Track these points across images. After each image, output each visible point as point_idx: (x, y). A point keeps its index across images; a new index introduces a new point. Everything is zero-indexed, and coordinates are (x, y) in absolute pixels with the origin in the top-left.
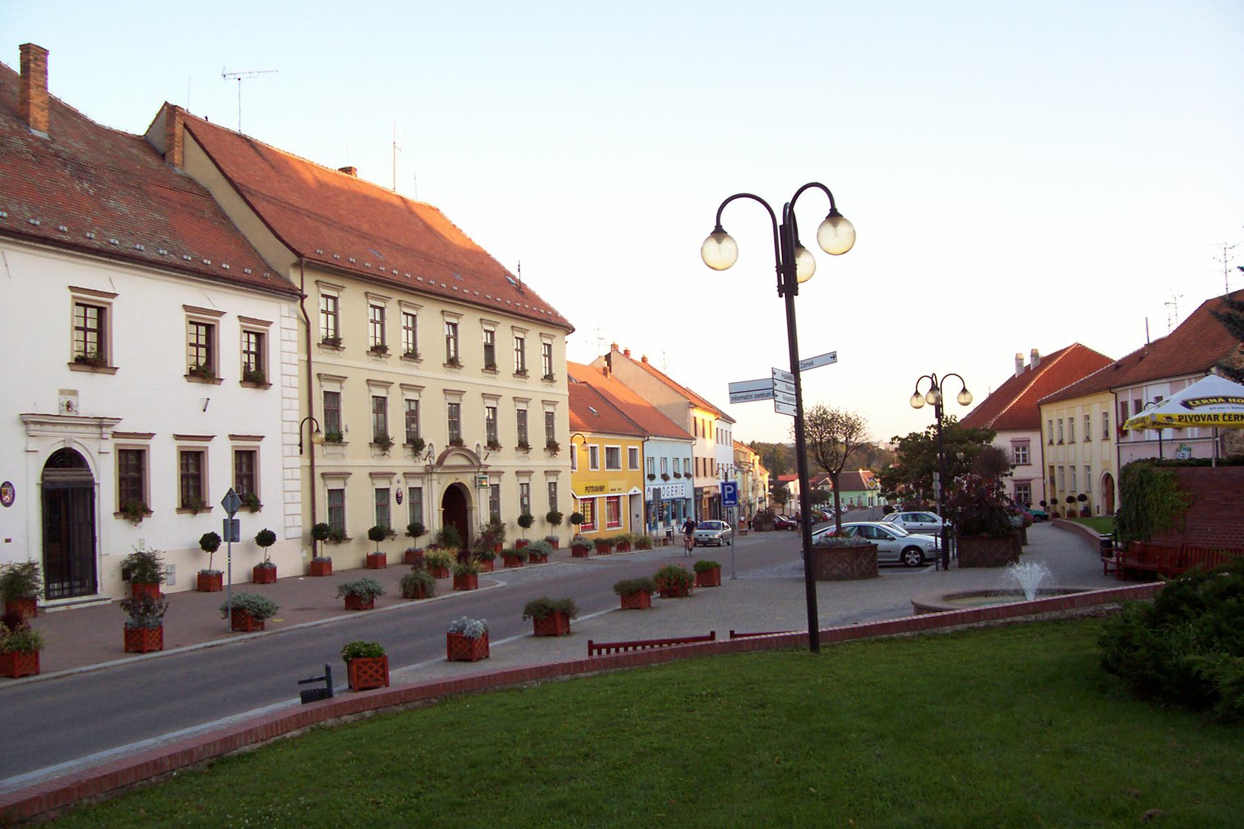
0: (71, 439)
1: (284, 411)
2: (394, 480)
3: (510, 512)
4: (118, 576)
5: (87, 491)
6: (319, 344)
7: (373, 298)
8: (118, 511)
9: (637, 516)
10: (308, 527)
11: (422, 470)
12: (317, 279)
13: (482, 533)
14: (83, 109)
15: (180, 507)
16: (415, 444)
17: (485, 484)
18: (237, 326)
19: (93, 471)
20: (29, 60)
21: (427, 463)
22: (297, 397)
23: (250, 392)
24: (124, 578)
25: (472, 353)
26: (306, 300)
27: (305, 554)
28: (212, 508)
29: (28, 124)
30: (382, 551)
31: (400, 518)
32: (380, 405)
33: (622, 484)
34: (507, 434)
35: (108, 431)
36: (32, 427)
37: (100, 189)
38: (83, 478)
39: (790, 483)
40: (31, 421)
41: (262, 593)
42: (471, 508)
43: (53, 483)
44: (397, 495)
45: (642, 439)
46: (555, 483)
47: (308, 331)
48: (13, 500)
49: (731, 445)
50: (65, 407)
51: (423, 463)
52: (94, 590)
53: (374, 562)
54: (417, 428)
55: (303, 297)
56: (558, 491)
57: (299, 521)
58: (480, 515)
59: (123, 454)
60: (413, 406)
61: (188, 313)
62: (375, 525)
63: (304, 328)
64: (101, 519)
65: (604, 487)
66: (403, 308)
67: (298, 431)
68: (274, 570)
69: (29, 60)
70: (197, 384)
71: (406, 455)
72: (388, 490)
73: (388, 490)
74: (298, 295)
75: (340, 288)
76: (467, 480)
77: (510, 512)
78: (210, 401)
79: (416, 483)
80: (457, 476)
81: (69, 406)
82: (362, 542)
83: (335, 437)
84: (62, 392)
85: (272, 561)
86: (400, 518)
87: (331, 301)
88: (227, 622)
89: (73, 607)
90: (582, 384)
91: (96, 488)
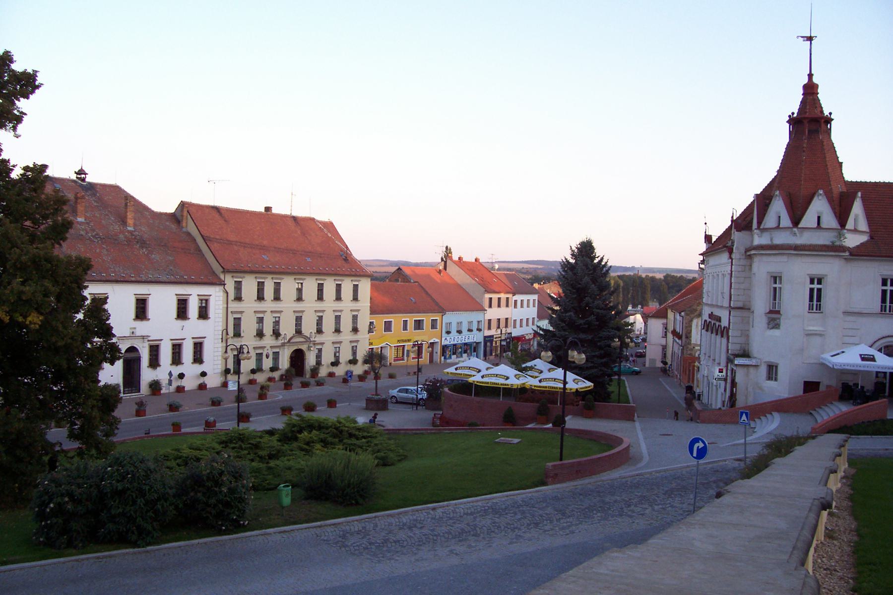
1: (823, 225)
2: (266, 349)
3: (328, 357)
4: (148, 386)
5: (138, 359)
6: (232, 300)
9: (436, 353)
10: (224, 369)
11: (280, 345)
13: (310, 369)
14: (150, 206)
16: (276, 334)
18: (197, 298)
19: (141, 353)
20: (127, 203)
21: (283, 341)
23: (202, 322)
24: (150, 388)
26: (226, 286)
27: (222, 379)
29: (126, 225)
30: (255, 378)
31: (267, 363)
32: (261, 320)
33: (425, 338)
34: (328, 325)
35: (146, 340)
36: (120, 341)
37: (149, 251)
39: (631, 317)
41: (178, 399)
42: (306, 359)
44: (267, 355)
45: (442, 314)
46: (356, 346)
47: (227, 296)
49: (534, 306)
51: (281, 342)
52: (139, 391)
53: (270, 379)
54: (279, 328)
55: (224, 285)
57: (220, 367)
58: (310, 360)
59: (151, 347)
60: (277, 319)
63: (226, 295)
65: (411, 340)
67: (221, 333)
68: (206, 385)
69: (127, 203)
72: (262, 353)
73: (262, 353)
74: (222, 284)
75: (342, 280)
76: (304, 347)
77: (328, 357)
79: (277, 350)
81: (133, 333)
82: (328, 366)
83: (237, 334)
84: (131, 328)
85: (206, 382)
86: (267, 363)
88: (168, 409)
90: (415, 283)
91: (141, 359)
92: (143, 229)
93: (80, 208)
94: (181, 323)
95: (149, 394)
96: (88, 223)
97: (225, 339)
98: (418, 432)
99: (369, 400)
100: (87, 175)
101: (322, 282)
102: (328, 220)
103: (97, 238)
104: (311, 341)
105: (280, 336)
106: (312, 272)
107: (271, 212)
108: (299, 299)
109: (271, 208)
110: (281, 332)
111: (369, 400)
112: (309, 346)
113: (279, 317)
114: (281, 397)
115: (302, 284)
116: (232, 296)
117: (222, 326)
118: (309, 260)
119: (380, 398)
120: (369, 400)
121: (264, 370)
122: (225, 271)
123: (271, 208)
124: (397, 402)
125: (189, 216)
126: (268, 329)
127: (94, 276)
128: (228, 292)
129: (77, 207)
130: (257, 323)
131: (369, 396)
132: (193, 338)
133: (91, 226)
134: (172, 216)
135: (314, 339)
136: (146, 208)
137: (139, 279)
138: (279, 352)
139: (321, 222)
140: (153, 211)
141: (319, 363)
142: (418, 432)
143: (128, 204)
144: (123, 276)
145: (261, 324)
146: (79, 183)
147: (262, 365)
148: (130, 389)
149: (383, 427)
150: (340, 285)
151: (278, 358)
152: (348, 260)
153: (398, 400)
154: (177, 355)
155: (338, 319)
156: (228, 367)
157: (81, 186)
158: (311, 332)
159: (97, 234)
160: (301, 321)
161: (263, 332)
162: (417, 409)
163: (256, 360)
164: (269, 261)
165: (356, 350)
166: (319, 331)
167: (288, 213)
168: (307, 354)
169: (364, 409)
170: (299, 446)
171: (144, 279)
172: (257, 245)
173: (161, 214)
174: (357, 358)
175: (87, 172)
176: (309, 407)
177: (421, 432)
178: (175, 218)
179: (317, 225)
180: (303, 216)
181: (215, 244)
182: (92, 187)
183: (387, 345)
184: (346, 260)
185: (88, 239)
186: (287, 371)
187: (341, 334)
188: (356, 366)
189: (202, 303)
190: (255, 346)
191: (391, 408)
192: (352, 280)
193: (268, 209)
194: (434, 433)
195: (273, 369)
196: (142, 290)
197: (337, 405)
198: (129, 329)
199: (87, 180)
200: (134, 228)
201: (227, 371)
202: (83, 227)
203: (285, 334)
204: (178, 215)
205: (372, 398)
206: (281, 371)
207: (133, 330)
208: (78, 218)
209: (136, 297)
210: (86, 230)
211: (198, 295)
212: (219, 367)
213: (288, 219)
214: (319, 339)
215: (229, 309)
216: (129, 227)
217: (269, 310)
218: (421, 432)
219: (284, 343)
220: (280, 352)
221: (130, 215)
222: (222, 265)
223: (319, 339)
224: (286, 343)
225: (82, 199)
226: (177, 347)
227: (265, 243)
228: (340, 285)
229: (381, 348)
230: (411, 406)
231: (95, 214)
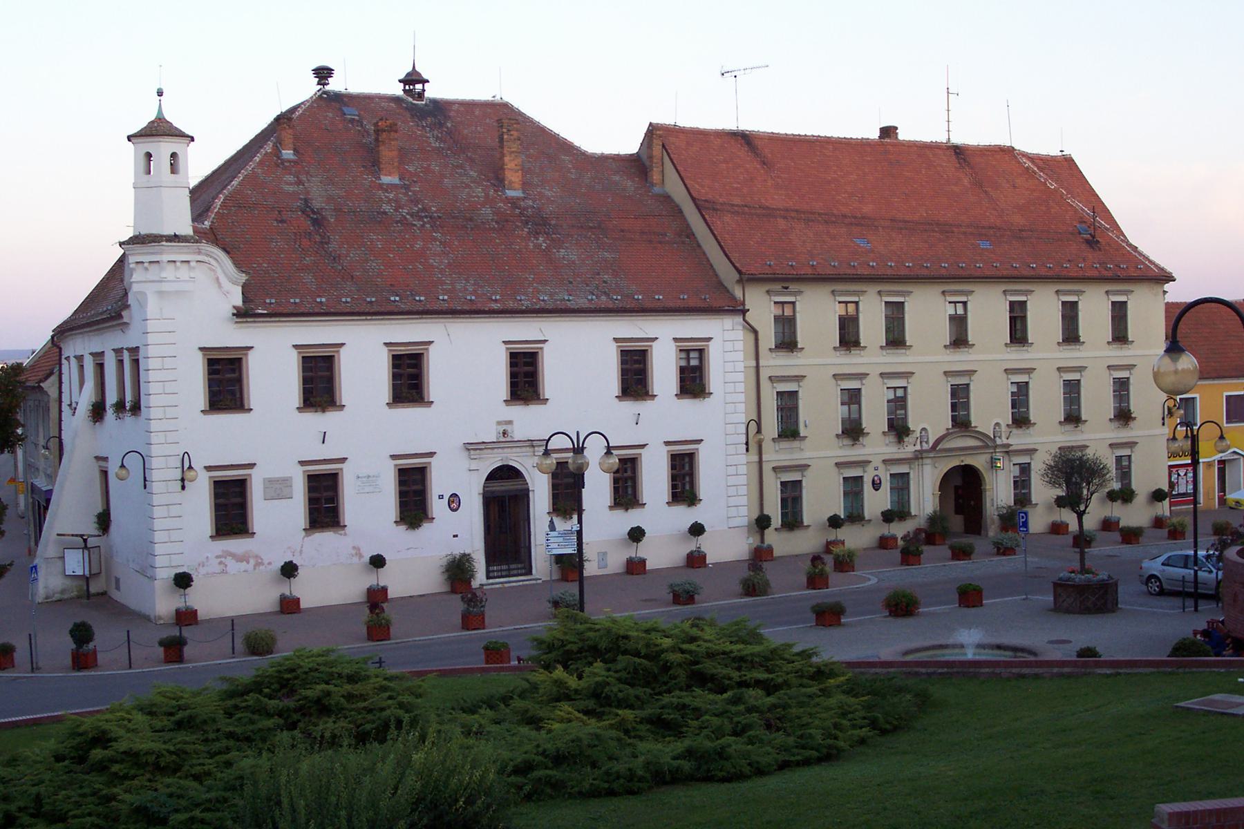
0: (507, 458)
2: (870, 469)
5: (522, 497)
7: (1011, 295)
8: (399, 520)
10: (755, 515)
11: (910, 456)
12: (767, 289)
15: (214, 534)
16: (898, 429)
17: (999, 465)
19: (528, 480)
21: (918, 447)
22: (744, 400)
23: (688, 404)
25: (872, 325)
26: (748, 314)
28: (346, 526)
31: (876, 502)
32: (853, 397)
36: (472, 452)
37: (553, 240)
38: (520, 487)
40: (472, 448)
43: (493, 492)
46: (1129, 456)
48: (459, 506)
50: (501, 435)
52: (530, 572)
54: (906, 414)
56: (1133, 466)
57: (744, 511)
60: (900, 393)
61: (508, 346)
62: (889, 507)
64: (536, 517)
66: (837, 298)
67: (744, 431)
68: (704, 557)
69: (502, 134)
70: (521, 406)
71: (887, 442)
74: (739, 309)
75: (1079, 293)
76: (979, 462)
78: (641, 416)
79: (903, 469)
80: (962, 458)
81: (504, 433)
82: (1049, 508)
83: (789, 431)
84: (499, 423)
86: (876, 502)
87: (960, 306)
89: (506, 585)
91: (531, 494)
92: (549, 194)
93: (387, 153)
94: (631, 407)
95: (555, 577)
96: (407, 188)
97: (753, 442)
98: (1025, 671)
99: (1060, 585)
100: (426, 85)
101: (1023, 298)
102: (1060, 154)
103: (421, 218)
104: (996, 447)
105: (908, 435)
106: (988, 273)
107: (897, 138)
108: (959, 340)
109: (896, 128)
110: (911, 426)
111: (1060, 587)
112: (992, 458)
113: (905, 388)
114: (874, 581)
115: (965, 303)
116: (768, 337)
117: (746, 413)
118: (985, 245)
119: (1089, 580)
120: (1060, 587)
121: (867, 517)
122: (746, 279)
123: (896, 128)
124: (1162, 593)
125: (665, 153)
126: (874, 417)
127: (395, 301)
128: (758, 329)
129: (378, 152)
130: (842, 404)
131: (1062, 575)
132: (667, 443)
133: (414, 192)
134: (635, 161)
135: (1005, 441)
136: (566, 147)
137: (511, 304)
138: (908, 474)
139: (1033, 158)
140: (584, 154)
141: (1023, 498)
142: (1025, 671)
143: (505, 137)
144: (471, 300)
145: (855, 407)
146: (407, 103)
147: (862, 506)
148: (504, 567)
149: (1035, 654)
150: (1124, 304)
151: (908, 488)
152: (1098, 242)
153: (1165, 586)
154: (629, 483)
155: (1072, 390)
156: (766, 512)
157: (413, 109)
158: (997, 424)
159: (424, 210)
160: (968, 397)
161: (861, 424)
162: (1196, 610)
163: (845, 494)
164: (872, 251)
165: (1129, 467)
166: (1021, 420)
167: (942, 138)
168: (987, 476)
169: (1051, 610)
170: (365, 700)
171: (526, 304)
172: (845, 216)
173: (603, 159)
174: (1134, 486)
175: (425, 76)
176: (896, 605)
177: (1036, 670)
178: (637, 165)
179: (1019, 163)
180: (982, 144)
181: (727, 218)
182: (440, 108)
183: (1236, 457)
184: (1092, 243)
185: (397, 222)
186: (932, 520)
187: (1081, 427)
188: (1130, 508)
189: (688, 359)
190: (887, 457)
191: (1123, 606)
192: (1057, 292)
193: (888, 132)
194: (1069, 676)
195: (888, 517)
196: (524, 330)
197: (984, 602)
198: (494, 426)
199: (427, 94)
200: (523, 193)
201: (762, 522)
202: (391, 196)
203: (924, 429)
204: (644, 157)
205: (1069, 579)
206: (917, 519)
207: (505, 427)
208: (382, 177)
209: (507, 349)
210: (397, 201)
211: (676, 340)
212: (744, 514)
213: (940, 152)
214: (1019, 439)
215: (761, 370)
216: (508, 189)
217: (874, 372)
218: (1036, 670)
219: (922, 452)
220: (912, 476)
221: (511, 163)
222: (737, 265)
223: (1019, 439)
224: (926, 451)
225: (389, 132)
226: (629, 465)
227: (868, 209)
228: (1074, 305)
229: (1222, 462)
230: (1177, 601)
231: (429, 165)
